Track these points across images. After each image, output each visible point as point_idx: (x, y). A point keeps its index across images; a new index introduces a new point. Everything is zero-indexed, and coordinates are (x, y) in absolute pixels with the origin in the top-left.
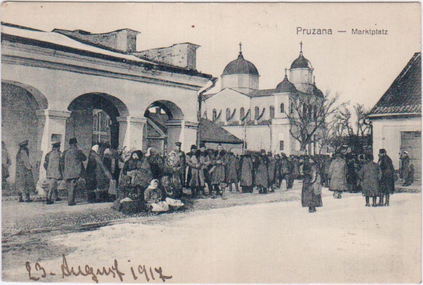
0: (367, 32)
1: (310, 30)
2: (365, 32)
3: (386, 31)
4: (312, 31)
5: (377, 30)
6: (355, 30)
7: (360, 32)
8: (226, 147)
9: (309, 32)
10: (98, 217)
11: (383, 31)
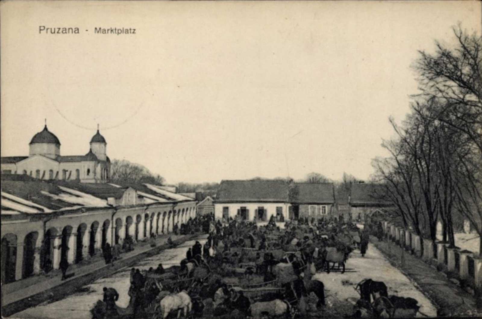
0: (112, 31)
1: (55, 29)
2: (109, 31)
3: (60, 33)
4: (57, 30)
5: (123, 29)
6: (98, 29)
7: (104, 31)
8: (150, 219)
9: (53, 31)
10: (269, 297)
11: (116, 29)
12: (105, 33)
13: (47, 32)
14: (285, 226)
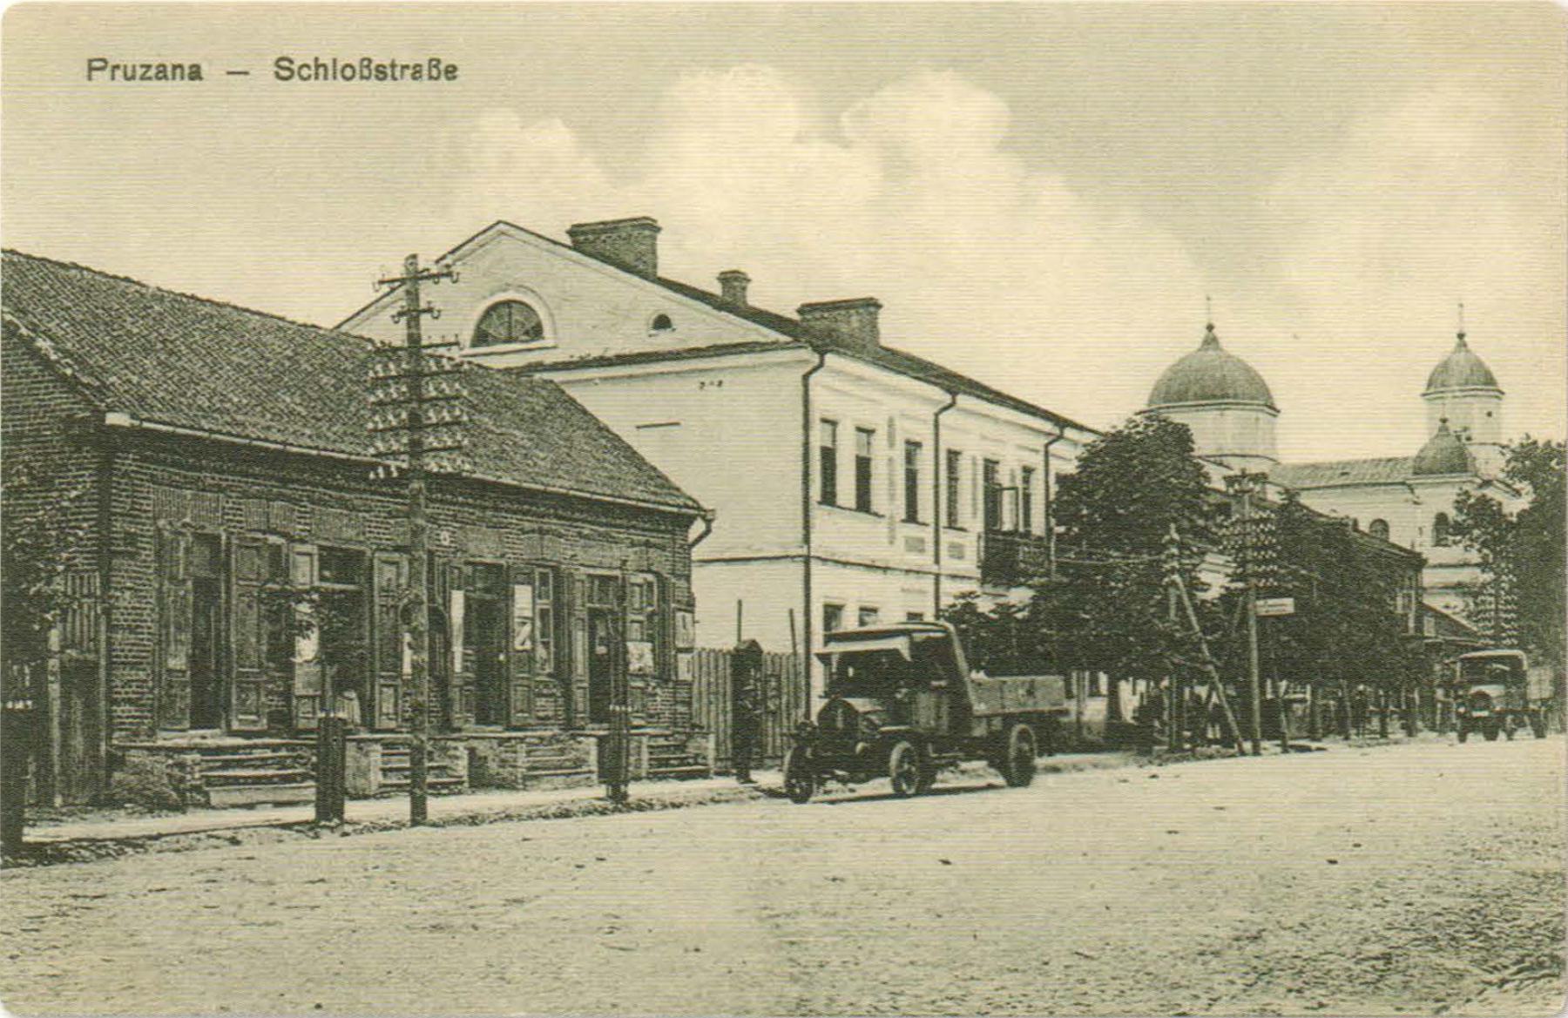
2: (408, 72)
4: (140, 71)
5: (335, 61)
11: (393, 66)
12: (165, 77)
13: (113, 78)
14: (625, 796)
